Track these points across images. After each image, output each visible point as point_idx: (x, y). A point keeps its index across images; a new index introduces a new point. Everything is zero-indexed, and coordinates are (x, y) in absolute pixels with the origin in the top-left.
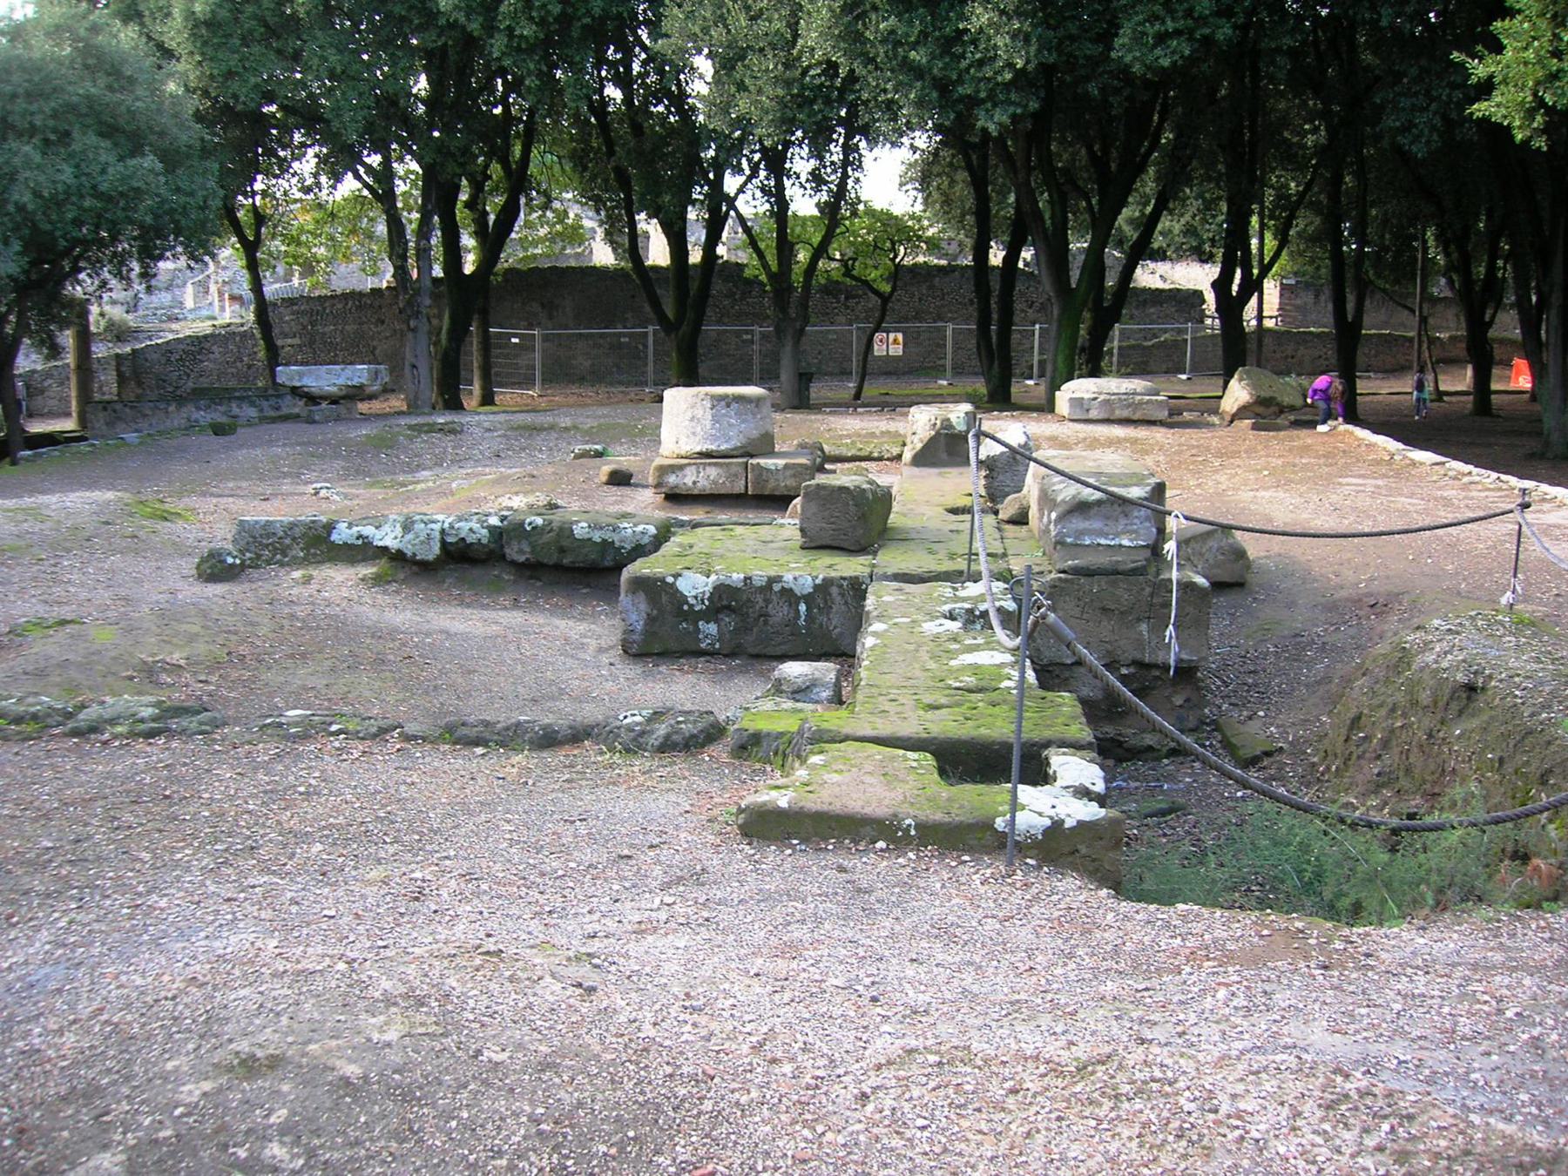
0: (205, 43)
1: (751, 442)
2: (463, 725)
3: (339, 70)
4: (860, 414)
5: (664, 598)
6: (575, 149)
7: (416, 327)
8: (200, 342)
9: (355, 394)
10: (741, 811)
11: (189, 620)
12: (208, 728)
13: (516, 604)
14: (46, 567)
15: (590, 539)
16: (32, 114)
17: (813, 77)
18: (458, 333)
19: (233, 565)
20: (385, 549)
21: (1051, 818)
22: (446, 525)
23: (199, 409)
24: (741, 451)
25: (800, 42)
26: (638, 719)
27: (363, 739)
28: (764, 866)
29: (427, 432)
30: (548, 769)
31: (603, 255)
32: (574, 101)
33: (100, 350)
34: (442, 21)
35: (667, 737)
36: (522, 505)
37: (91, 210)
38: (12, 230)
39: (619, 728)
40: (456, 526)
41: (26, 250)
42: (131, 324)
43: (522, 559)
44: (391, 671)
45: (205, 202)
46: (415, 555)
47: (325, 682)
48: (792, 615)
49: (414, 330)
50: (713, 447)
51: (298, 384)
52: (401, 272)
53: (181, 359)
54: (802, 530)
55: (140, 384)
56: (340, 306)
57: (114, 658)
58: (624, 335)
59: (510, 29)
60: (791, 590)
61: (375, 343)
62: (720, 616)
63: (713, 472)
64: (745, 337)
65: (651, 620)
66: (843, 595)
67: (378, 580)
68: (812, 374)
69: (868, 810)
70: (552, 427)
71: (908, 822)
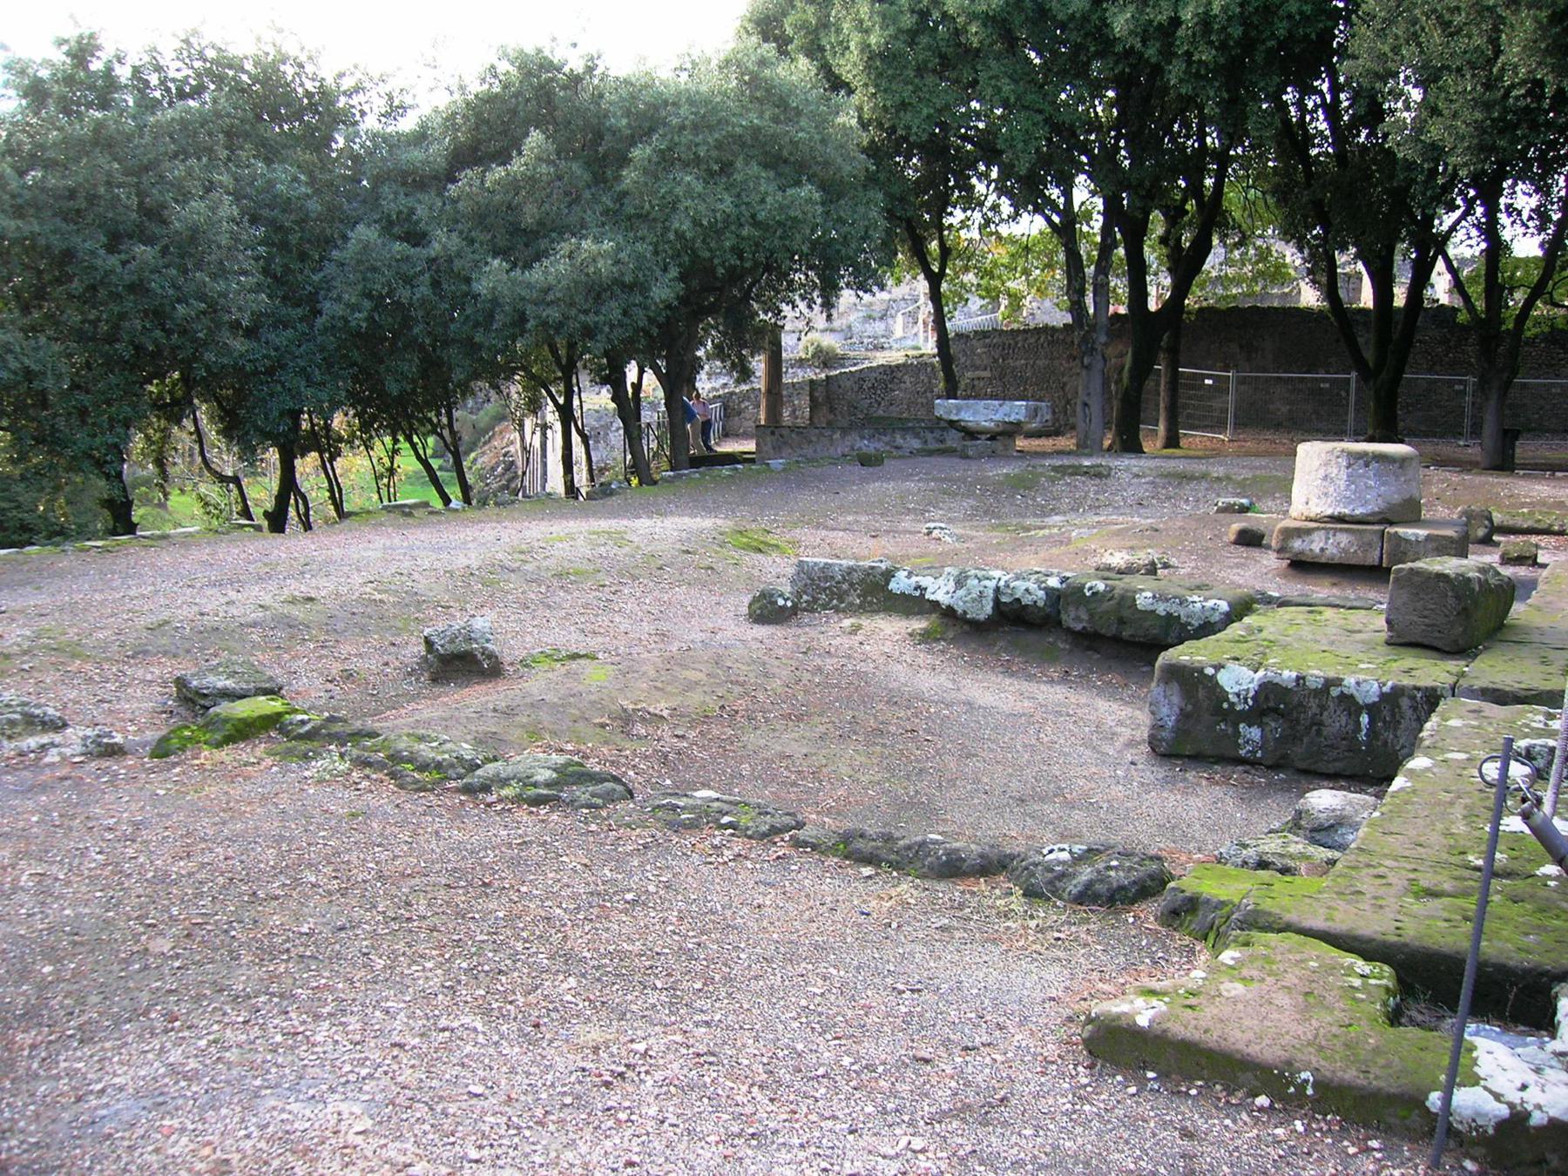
0: (880, 75)
1: (1392, 508)
2: (861, 836)
3: (1012, 100)
4: (1559, 479)
5: (1201, 694)
6: (1279, 185)
7: (1090, 364)
8: (892, 372)
9: (1009, 431)
10: (1090, 1020)
11: (696, 666)
12: (599, 801)
13: (1065, 679)
14: (605, 594)
15: (1153, 612)
16: (697, 145)
17: (1517, 98)
18: (1142, 370)
19: (783, 608)
20: (936, 604)
21: (1511, 1105)
22: (1002, 583)
23: (862, 438)
24: (1380, 517)
25: (1502, 59)
26: (1065, 856)
27: (750, 837)
28: (1087, 1108)
29: (1071, 475)
30: (933, 907)
31: (1310, 297)
32: (1257, 130)
33: (791, 377)
34: (1119, 48)
35: (1089, 885)
36: (1122, 562)
37: (749, 238)
38: (672, 258)
39: (1036, 865)
40: (1012, 585)
41: (683, 277)
42: (838, 351)
43: (1078, 627)
44: (884, 745)
45: (866, 232)
46: (965, 613)
47: (804, 751)
48: (1351, 727)
49: (1088, 368)
50: (1347, 511)
51: (955, 418)
52: (1077, 308)
53: (873, 387)
54: (1388, 622)
55: (832, 410)
56: (1033, 340)
57: (592, 703)
58: (1324, 380)
59: (1188, 54)
60: (1352, 696)
61: (1065, 379)
62: (1265, 720)
63: (1344, 539)
64: (1456, 387)
65: (1184, 716)
66: (1415, 709)
67: (926, 637)
68: (1519, 431)
69: (1254, 1050)
70: (1204, 477)
71: (1304, 1075)
